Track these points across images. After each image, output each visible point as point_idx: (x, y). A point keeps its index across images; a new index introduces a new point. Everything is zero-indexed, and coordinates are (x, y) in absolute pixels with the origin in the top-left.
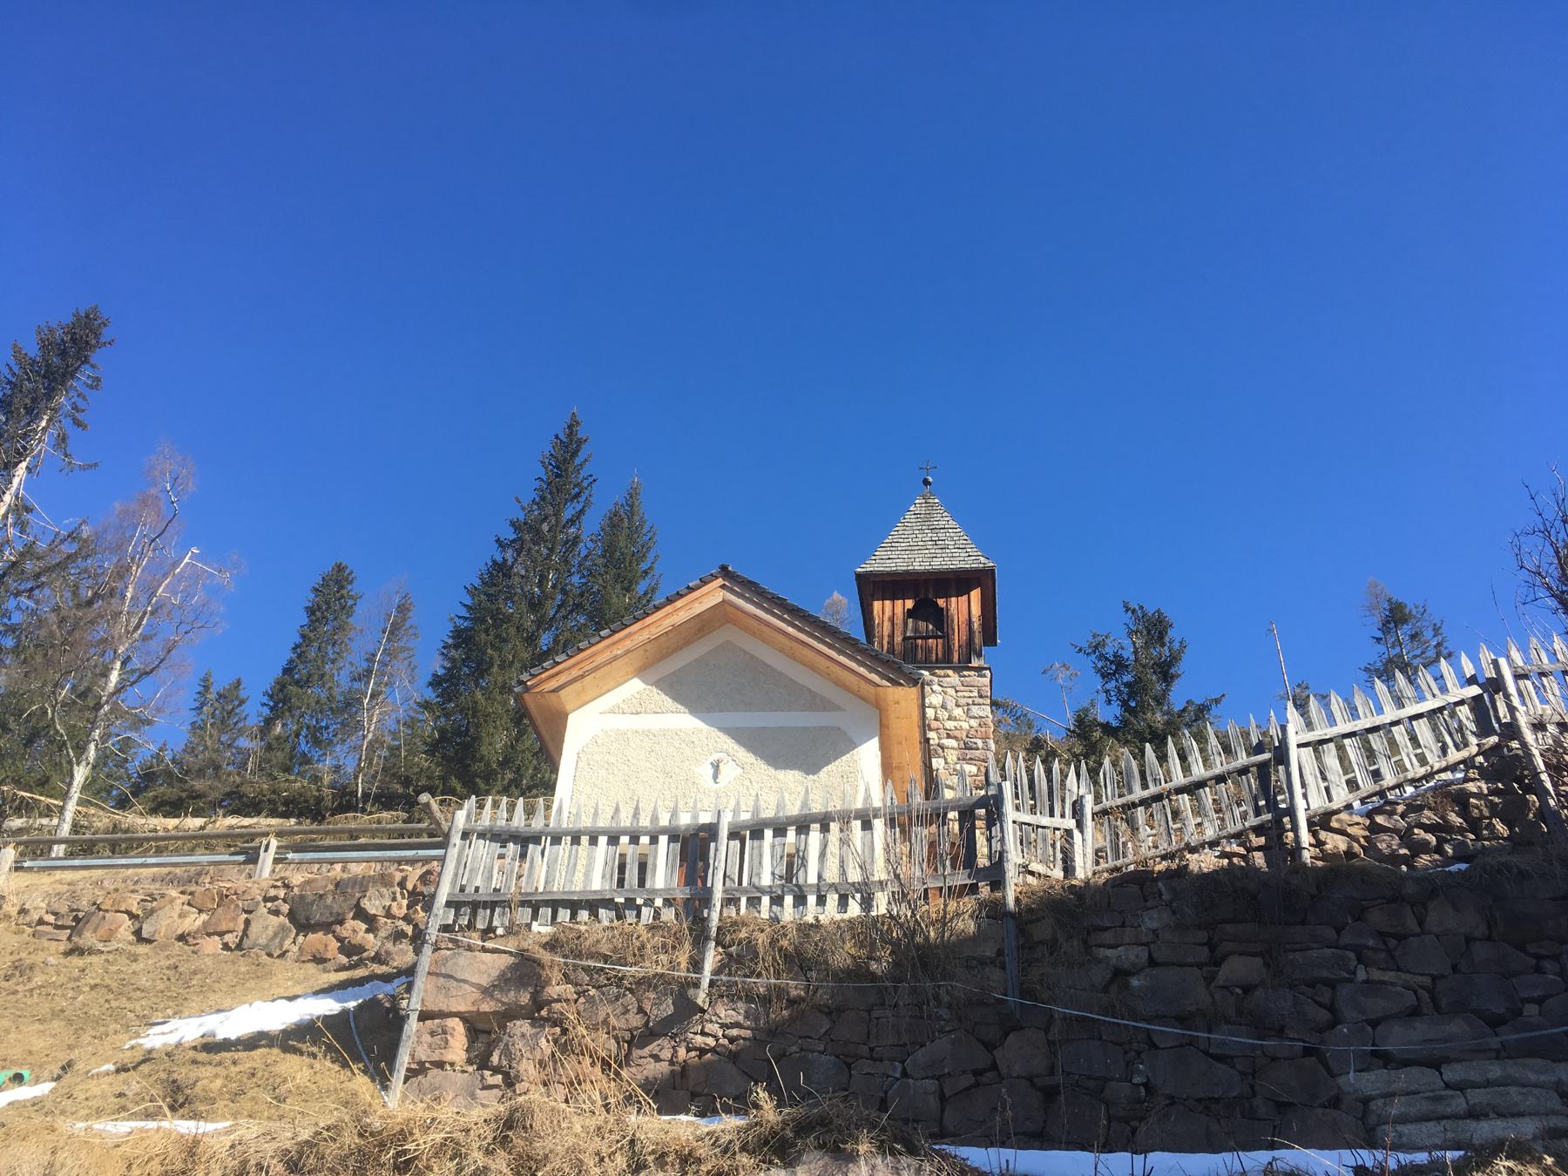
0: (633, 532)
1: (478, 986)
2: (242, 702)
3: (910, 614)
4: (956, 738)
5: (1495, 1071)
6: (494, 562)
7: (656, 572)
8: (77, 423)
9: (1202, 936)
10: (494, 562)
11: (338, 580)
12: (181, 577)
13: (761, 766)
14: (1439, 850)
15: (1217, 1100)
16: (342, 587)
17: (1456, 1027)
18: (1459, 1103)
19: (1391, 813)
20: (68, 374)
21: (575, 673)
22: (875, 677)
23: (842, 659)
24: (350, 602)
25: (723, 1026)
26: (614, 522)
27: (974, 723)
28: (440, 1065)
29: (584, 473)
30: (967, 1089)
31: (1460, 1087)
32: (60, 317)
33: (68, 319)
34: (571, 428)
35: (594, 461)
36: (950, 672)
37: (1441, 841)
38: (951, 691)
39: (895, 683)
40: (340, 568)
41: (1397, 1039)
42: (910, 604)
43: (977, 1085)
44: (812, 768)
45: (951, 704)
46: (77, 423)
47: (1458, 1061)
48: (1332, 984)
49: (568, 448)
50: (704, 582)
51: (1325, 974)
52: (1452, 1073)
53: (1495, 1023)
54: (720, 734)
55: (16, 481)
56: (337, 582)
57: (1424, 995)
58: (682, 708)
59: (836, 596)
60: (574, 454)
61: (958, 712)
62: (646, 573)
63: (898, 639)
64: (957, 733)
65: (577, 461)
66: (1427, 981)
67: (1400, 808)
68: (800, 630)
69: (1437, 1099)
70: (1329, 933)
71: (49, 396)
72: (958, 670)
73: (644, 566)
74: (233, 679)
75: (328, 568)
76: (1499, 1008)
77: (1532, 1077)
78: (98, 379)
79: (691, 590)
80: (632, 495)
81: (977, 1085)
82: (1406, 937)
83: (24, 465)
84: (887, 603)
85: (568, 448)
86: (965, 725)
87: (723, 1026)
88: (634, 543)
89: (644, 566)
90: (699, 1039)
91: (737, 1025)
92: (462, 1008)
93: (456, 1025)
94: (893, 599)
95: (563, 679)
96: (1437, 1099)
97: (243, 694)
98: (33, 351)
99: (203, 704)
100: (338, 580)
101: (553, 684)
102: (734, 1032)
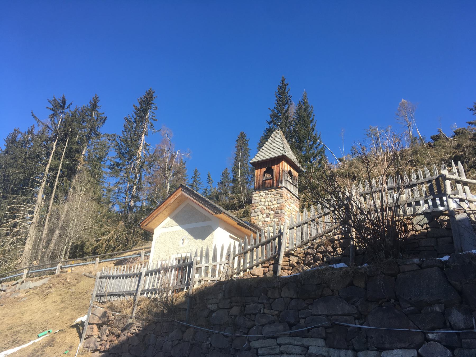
0: (306, 110)
1: (98, 317)
2: (229, 174)
3: (265, 172)
4: (273, 211)
5: (287, 340)
6: (267, 129)
7: (314, 120)
8: (155, 120)
9: (228, 301)
10: (267, 129)
11: (242, 136)
12: (177, 158)
13: (193, 239)
14: (323, 259)
15: (223, 348)
16: (243, 139)
17: (280, 327)
18: (277, 351)
19: (313, 248)
20: (149, 107)
21: (150, 220)
22: (212, 212)
23: (206, 208)
24: (246, 142)
25: (137, 327)
26: (299, 108)
27: (278, 205)
28: (92, 336)
29: (288, 95)
30: (177, 344)
31: (280, 345)
32: (142, 94)
33: (145, 94)
34: (283, 80)
35: (291, 90)
36: (273, 190)
37: (323, 256)
38: (273, 196)
39: (217, 214)
40: (242, 133)
41: (267, 330)
42: (265, 169)
43: (179, 343)
44: (203, 239)
45: (273, 200)
46: (155, 120)
47: (279, 337)
48: (255, 314)
49: (283, 89)
50: (177, 190)
51: (252, 312)
52: (279, 341)
53: (291, 326)
54: (185, 231)
55: (143, 140)
56: (242, 137)
57: (276, 317)
58: (177, 224)
59: (403, 100)
60: (285, 88)
61: (275, 202)
62: (312, 121)
63: (261, 181)
64: (273, 209)
65: (286, 91)
66: (277, 312)
67: (315, 246)
68: (197, 200)
69: (272, 349)
70: (256, 299)
71: (145, 116)
72: (275, 189)
73: (311, 119)
74: (225, 169)
75: (239, 134)
76: (292, 321)
77: (296, 343)
78: (156, 107)
79: (174, 192)
80: (305, 97)
81: (179, 343)
82: (275, 299)
83: (143, 135)
84: (259, 170)
85: (283, 89)
86: (276, 206)
87: (137, 327)
88: (307, 112)
89: (311, 119)
90: (132, 330)
91: (139, 327)
92: (96, 322)
93: (95, 326)
94: (261, 168)
95: (147, 222)
96: (272, 349)
97: (228, 172)
98: (138, 105)
99: (209, 181)
100: (242, 136)
101: (145, 224)
102: (139, 328)
